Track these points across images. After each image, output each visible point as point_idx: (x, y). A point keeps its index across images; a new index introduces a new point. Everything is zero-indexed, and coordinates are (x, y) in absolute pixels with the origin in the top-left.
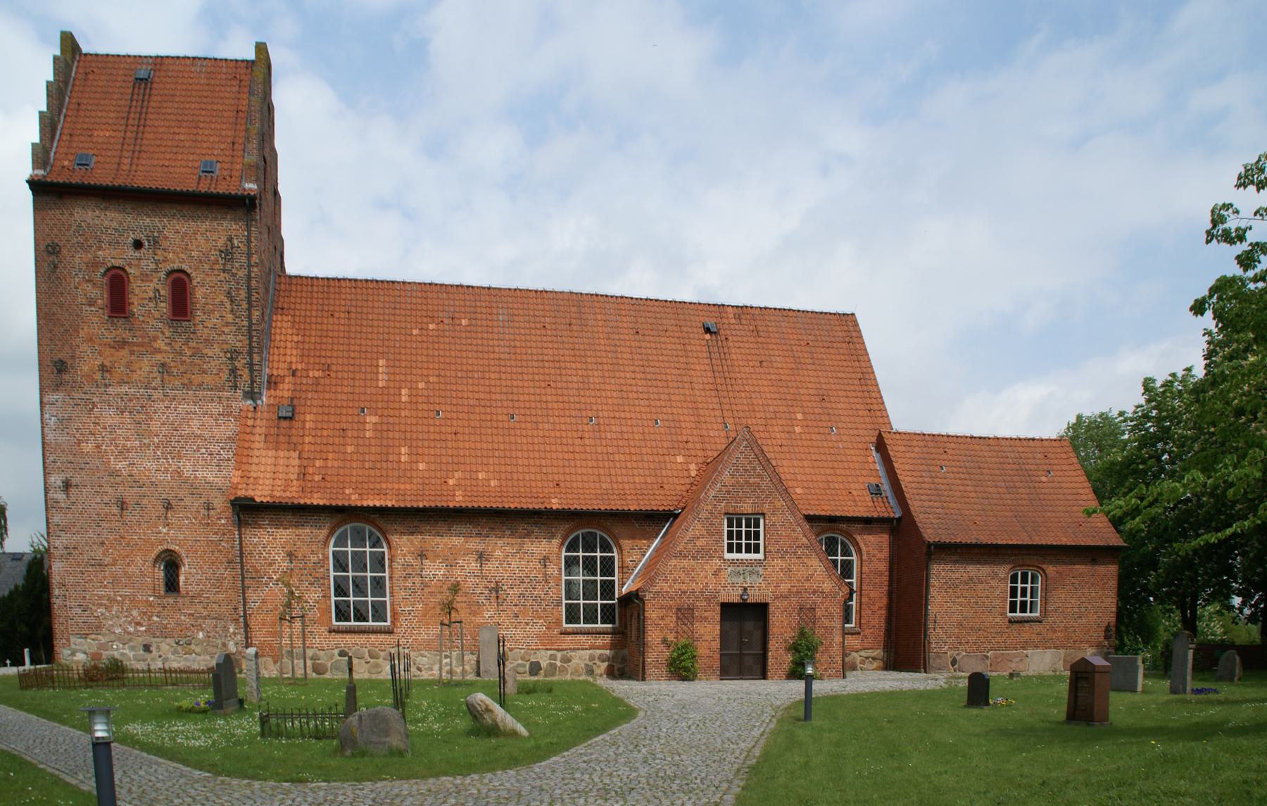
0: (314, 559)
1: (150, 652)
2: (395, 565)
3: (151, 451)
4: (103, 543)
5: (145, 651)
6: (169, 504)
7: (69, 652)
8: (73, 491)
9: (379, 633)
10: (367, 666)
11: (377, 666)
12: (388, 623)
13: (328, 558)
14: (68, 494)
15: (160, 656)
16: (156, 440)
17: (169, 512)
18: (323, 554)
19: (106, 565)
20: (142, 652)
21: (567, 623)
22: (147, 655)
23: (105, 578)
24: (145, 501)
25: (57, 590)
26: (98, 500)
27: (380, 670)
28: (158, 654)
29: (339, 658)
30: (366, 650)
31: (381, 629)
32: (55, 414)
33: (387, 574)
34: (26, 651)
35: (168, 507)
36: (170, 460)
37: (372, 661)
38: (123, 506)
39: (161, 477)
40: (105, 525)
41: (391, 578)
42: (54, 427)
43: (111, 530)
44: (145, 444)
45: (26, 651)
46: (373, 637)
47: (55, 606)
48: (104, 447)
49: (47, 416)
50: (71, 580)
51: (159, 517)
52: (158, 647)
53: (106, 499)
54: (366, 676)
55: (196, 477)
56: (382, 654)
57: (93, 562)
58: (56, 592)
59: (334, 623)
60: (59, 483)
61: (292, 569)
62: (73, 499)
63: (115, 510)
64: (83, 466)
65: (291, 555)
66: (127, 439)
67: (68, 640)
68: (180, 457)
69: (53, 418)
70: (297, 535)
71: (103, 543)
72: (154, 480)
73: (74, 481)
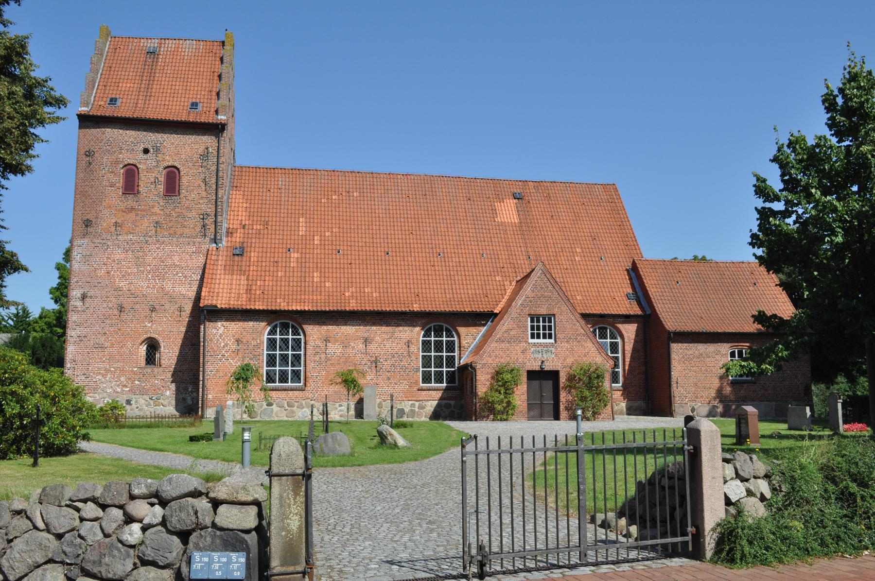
0: (254, 343)
2: (308, 347)
4: (105, 334)
10: (285, 412)
11: (293, 412)
12: (457, 384)
13: (263, 342)
15: (137, 408)
16: (148, 268)
23: (104, 356)
24: (137, 307)
26: (105, 306)
28: (136, 406)
33: (302, 353)
37: (289, 409)
38: (121, 309)
39: (150, 291)
40: (108, 322)
41: (305, 354)
53: (110, 305)
55: (174, 291)
56: (296, 404)
57: (97, 346)
60: (79, 295)
62: (87, 305)
63: (116, 312)
66: (129, 268)
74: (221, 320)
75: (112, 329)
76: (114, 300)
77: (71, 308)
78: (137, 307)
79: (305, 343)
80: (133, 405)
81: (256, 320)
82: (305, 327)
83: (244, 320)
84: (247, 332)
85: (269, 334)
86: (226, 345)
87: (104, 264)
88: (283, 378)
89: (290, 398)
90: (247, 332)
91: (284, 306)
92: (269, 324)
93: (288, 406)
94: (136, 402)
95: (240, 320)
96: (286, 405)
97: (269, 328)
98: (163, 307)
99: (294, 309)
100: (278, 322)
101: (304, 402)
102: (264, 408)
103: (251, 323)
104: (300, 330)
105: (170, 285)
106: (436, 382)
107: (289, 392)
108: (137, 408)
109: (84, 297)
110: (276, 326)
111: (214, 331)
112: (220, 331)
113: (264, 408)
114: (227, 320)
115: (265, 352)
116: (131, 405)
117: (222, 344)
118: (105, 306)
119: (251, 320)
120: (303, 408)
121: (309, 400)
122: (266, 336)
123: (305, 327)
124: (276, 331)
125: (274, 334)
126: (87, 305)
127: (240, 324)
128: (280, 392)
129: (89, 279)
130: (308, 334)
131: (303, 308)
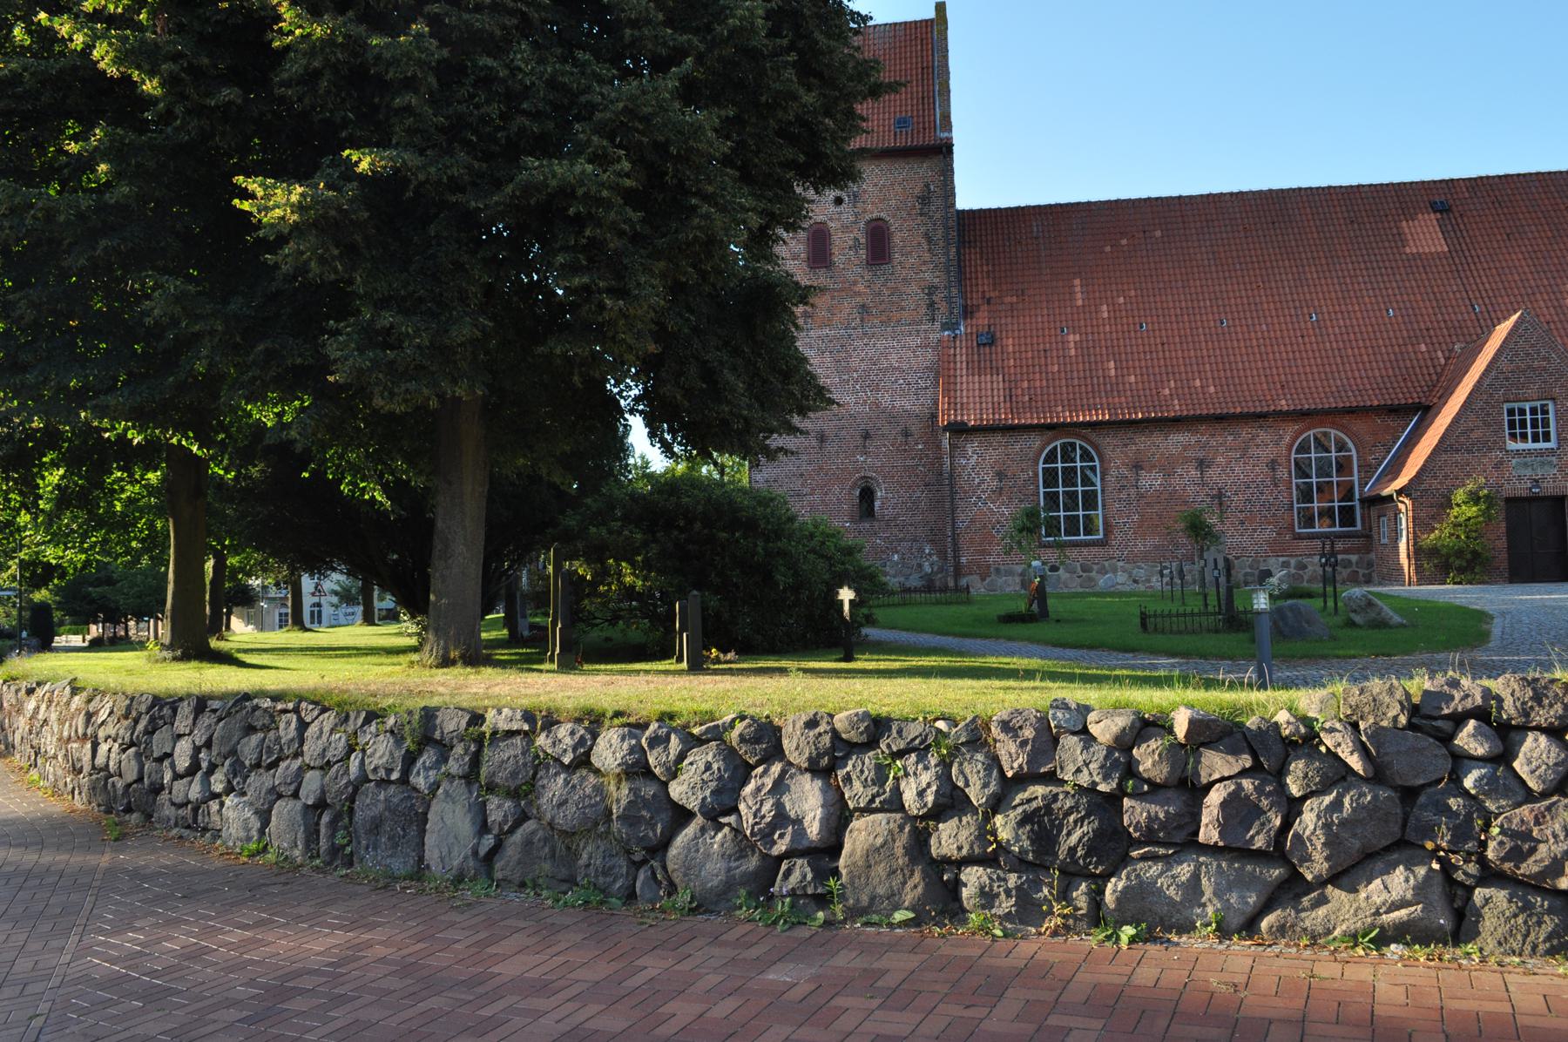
0: (1024, 476)
10: (1079, 580)
11: (1090, 579)
16: (855, 375)
33: (1099, 488)
39: (860, 409)
41: (1103, 491)
55: (894, 407)
56: (1095, 567)
65: (1000, 475)
86: (983, 481)
101: (1106, 564)
112: (973, 461)
122: (1041, 466)
130: (1108, 452)
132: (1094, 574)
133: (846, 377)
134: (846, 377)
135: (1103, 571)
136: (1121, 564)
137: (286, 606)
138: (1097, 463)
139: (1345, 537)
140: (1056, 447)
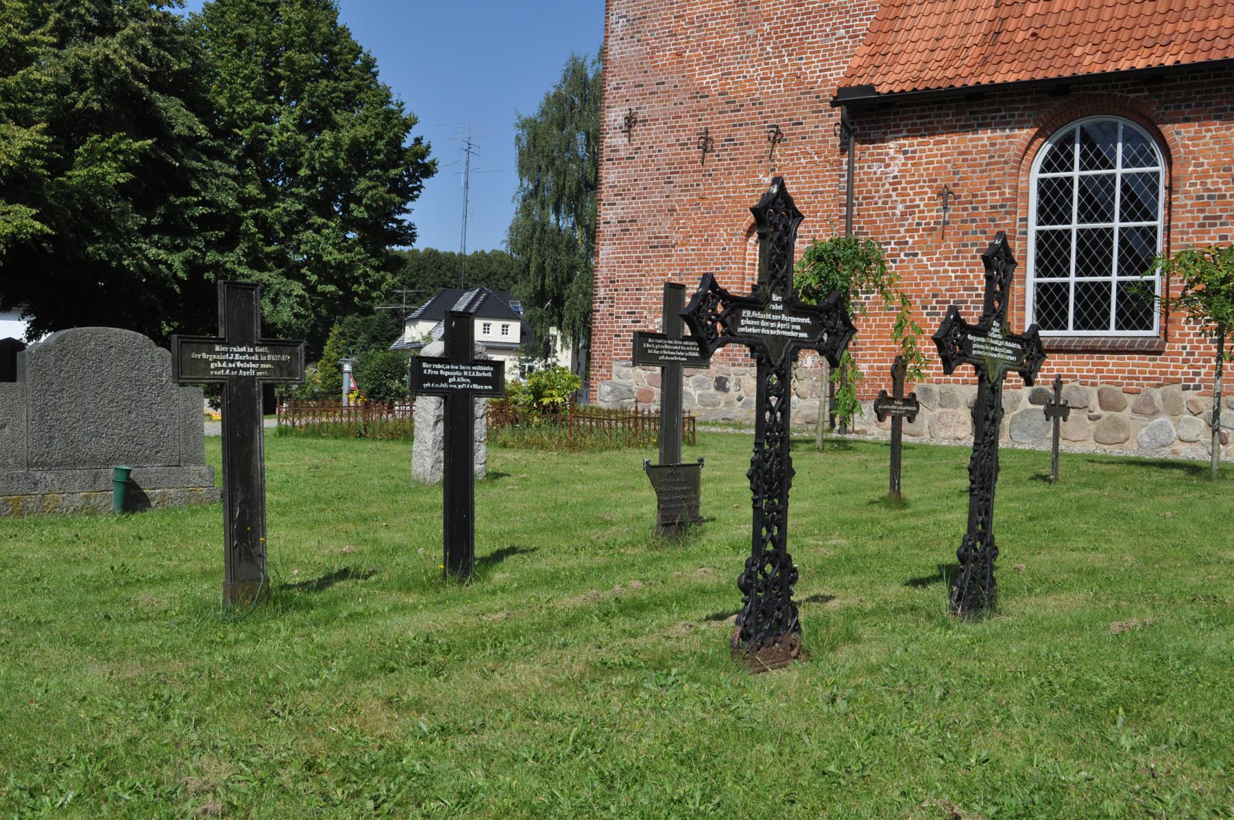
0: (993, 198)
1: (726, 390)
2: (1179, 199)
3: (758, 48)
4: (672, 210)
5: (717, 388)
6: (778, 132)
7: (609, 389)
8: (638, 128)
9: (1127, 352)
10: (1092, 426)
11: (1118, 426)
12: (1154, 332)
13: (1026, 195)
14: (630, 136)
15: (740, 399)
16: (766, 27)
17: (777, 148)
18: (1015, 188)
19: (673, 246)
20: (712, 390)
21: (1149, 328)
22: (721, 396)
23: (669, 266)
24: (740, 134)
25: (602, 290)
26: (672, 140)
27: (1122, 436)
28: (737, 395)
29: (1031, 406)
30: (1094, 392)
31: (1141, 344)
32: (624, 14)
33: (1160, 223)
34: (490, 387)
35: (776, 137)
36: (786, 58)
37: (1105, 414)
38: (706, 144)
39: (769, 87)
40: (678, 179)
41: (1168, 228)
42: (621, 34)
43: (685, 189)
44: (748, 37)
45: (490, 387)
46: (1109, 359)
47: (598, 316)
48: (688, 53)
49: (613, 19)
50: (622, 272)
51: (760, 159)
52: (738, 383)
53: (684, 138)
54: (1091, 447)
55: (825, 81)
56: (1131, 400)
57: (655, 242)
58: (601, 293)
59: (1154, 332)
60: (621, 121)
61: (946, 223)
62: (637, 144)
63: (695, 153)
64: (655, 88)
65: (945, 195)
66: (723, 34)
67: (609, 369)
68: (802, 51)
69: (621, 20)
70: (960, 154)
71: (672, 210)
72: (757, 96)
73: (640, 117)
74: (896, 133)
75: (685, 198)
76: (689, 122)
77: (606, 153)
78: (740, 134)
79: (1170, 189)
80: (732, 391)
81: (1002, 125)
82: (1168, 130)
83: (966, 128)
84: (974, 165)
85: (1047, 166)
86: (911, 209)
87: (672, 34)
88: (1092, 315)
89: (1110, 379)
90: (974, 165)
91: (1090, 63)
92: (1043, 133)
93: (1103, 406)
94: (738, 383)
95: (950, 129)
96: (1094, 402)
97: (1047, 147)
98: (799, 129)
99: (1124, 66)
100: (1076, 126)
101: (1157, 394)
102: (1020, 408)
103: (985, 136)
104: (1154, 145)
105: (816, 64)
106: (1123, 324)
107: (1106, 358)
108: (740, 399)
109: (630, 121)
110: (1069, 139)
111: (877, 169)
112: (895, 169)
113: (1020, 408)
114: (913, 132)
115: (1033, 228)
116: (726, 390)
117: (900, 207)
118: (672, 140)
119: (984, 126)
120: (1155, 413)
121: (1177, 388)
122: (1035, 175)
123: (1168, 130)
124: (1070, 156)
125: (1063, 167)
126: (637, 144)
127: (953, 140)
128: (1075, 358)
129: (640, 79)
130: (1178, 153)
131: (1154, 62)
132: (1126, 414)
133: (750, 32)
134: (750, 32)
135: (1147, 410)
136: (1190, 395)
137: (754, 270)
138: (1161, 168)
139: (1169, 215)
140: (1073, 132)
